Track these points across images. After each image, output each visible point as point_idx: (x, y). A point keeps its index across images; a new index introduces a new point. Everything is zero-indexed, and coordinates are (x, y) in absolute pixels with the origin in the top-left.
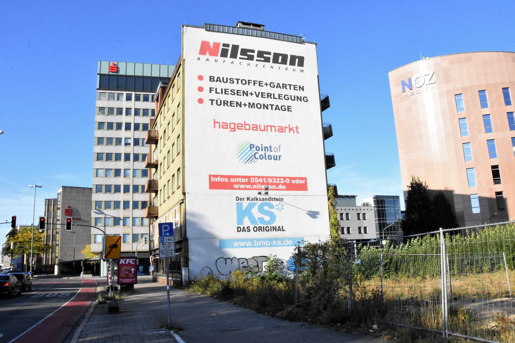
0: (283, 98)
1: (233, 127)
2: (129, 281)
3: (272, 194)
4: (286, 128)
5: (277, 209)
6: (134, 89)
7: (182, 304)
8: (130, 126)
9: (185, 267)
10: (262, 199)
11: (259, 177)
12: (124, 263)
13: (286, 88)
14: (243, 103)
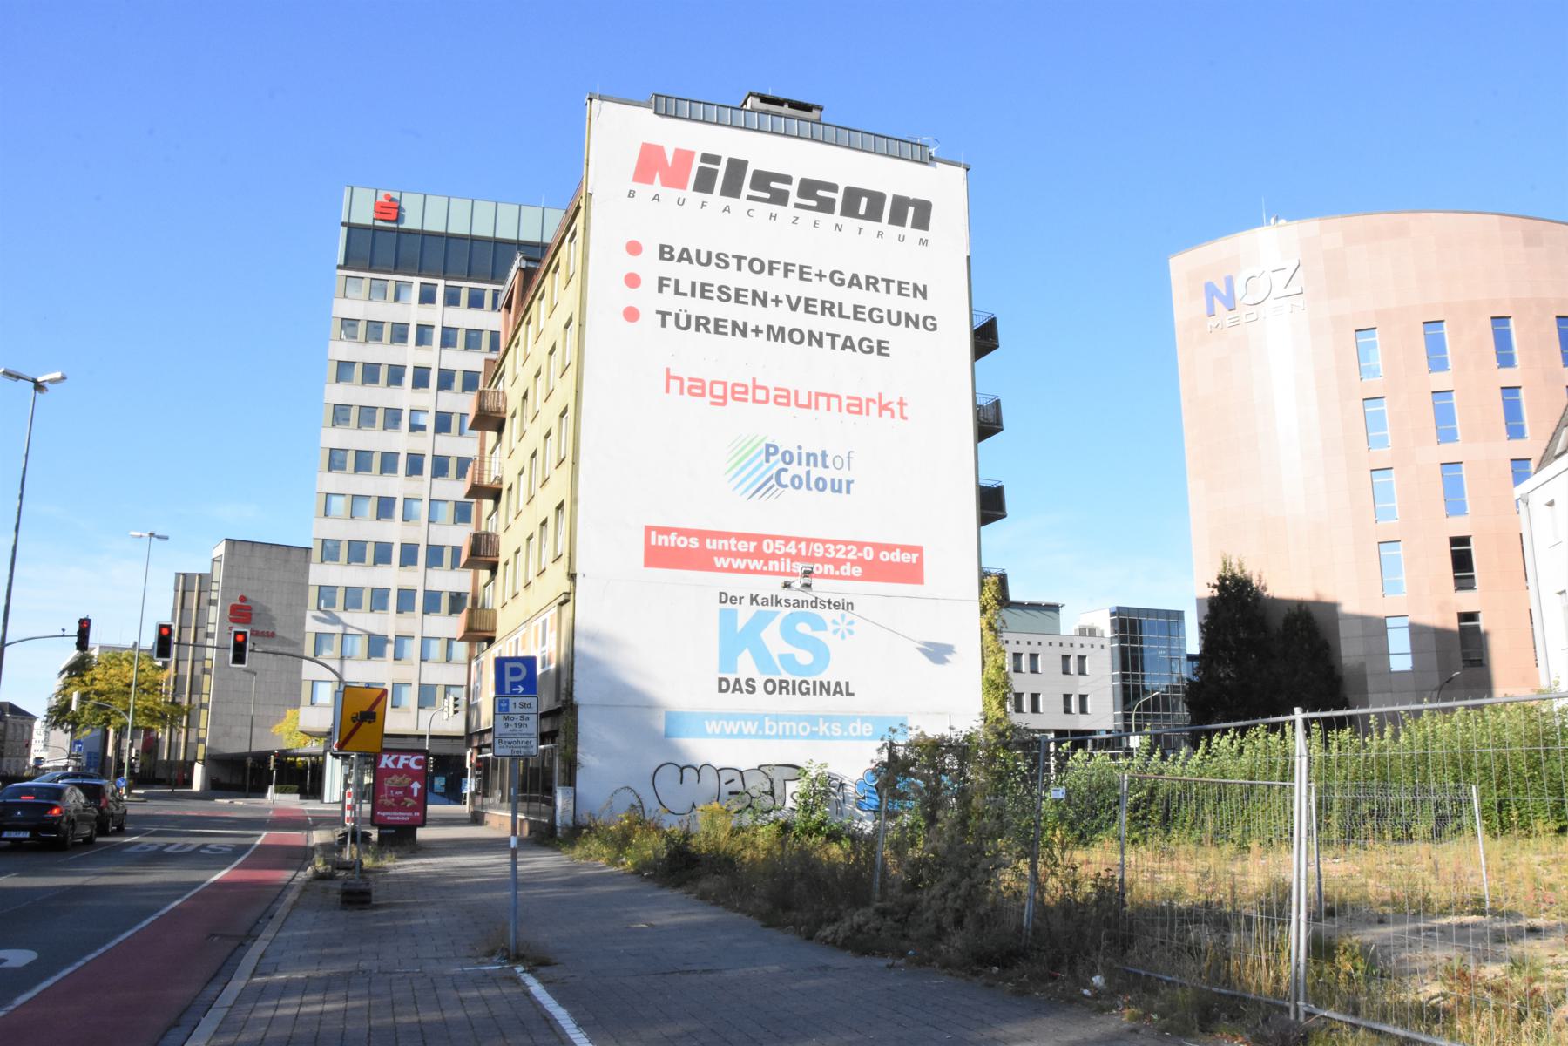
0: (866, 316)
2: (403, 819)
4: (871, 404)
5: (835, 632)
6: (445, 272)
9: (565, 784)
10: (792, 603)
11: (787, 540)
12: (391, 766)
13: (877, 290)
14: (751, 327)
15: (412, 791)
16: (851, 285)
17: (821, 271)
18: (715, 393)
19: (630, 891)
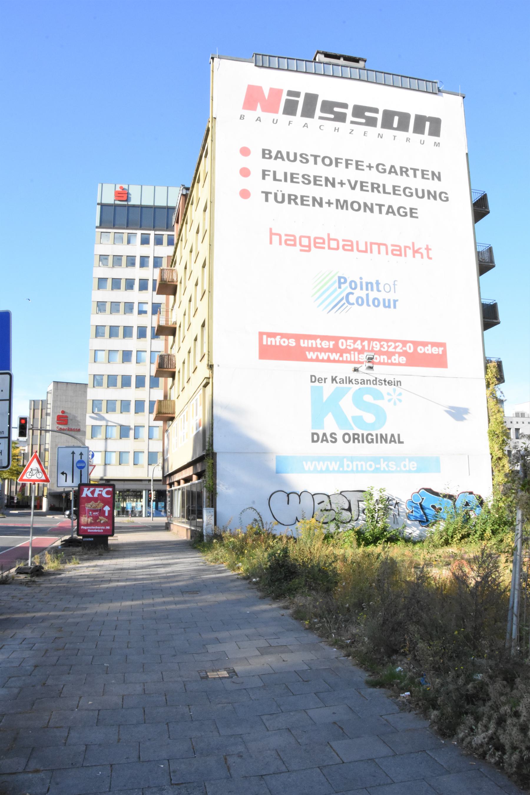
0: (401, 192)
1: (307, 244)
2: (99, 531)
3: (380, 372)
4: (407, 249)
5: (389, 400)
6: (154, 227)
7: (171, 599)
8: (147, 284)
9: (209, 506)
10: (360, 381)
11: (355, 340)
12: (90, 495)
13: (407, 175)
14: (325, 200)
15: (104, 512)
16: (390, 172)
17: (370, 164)
18: (303, 244)
19: (239, 602)
